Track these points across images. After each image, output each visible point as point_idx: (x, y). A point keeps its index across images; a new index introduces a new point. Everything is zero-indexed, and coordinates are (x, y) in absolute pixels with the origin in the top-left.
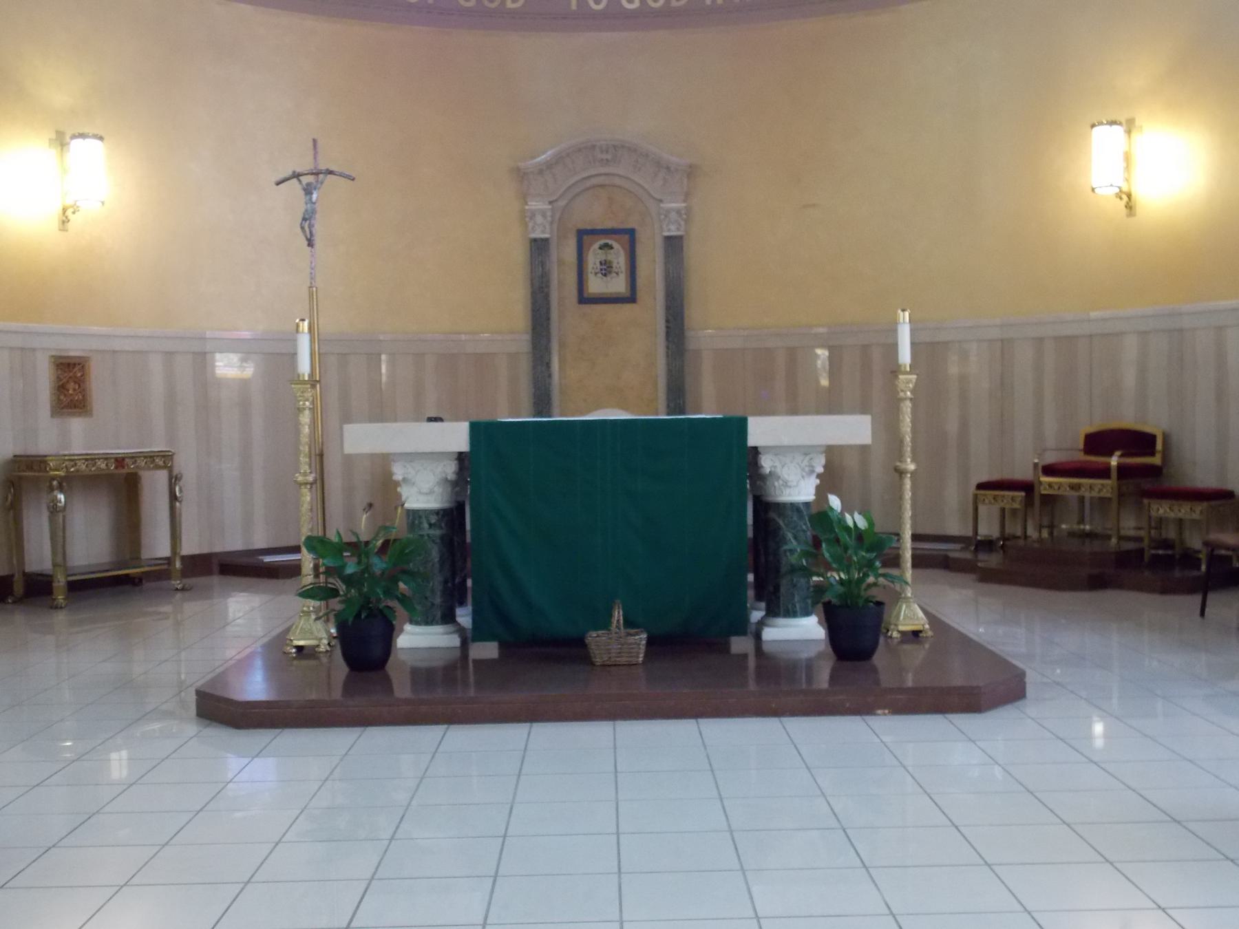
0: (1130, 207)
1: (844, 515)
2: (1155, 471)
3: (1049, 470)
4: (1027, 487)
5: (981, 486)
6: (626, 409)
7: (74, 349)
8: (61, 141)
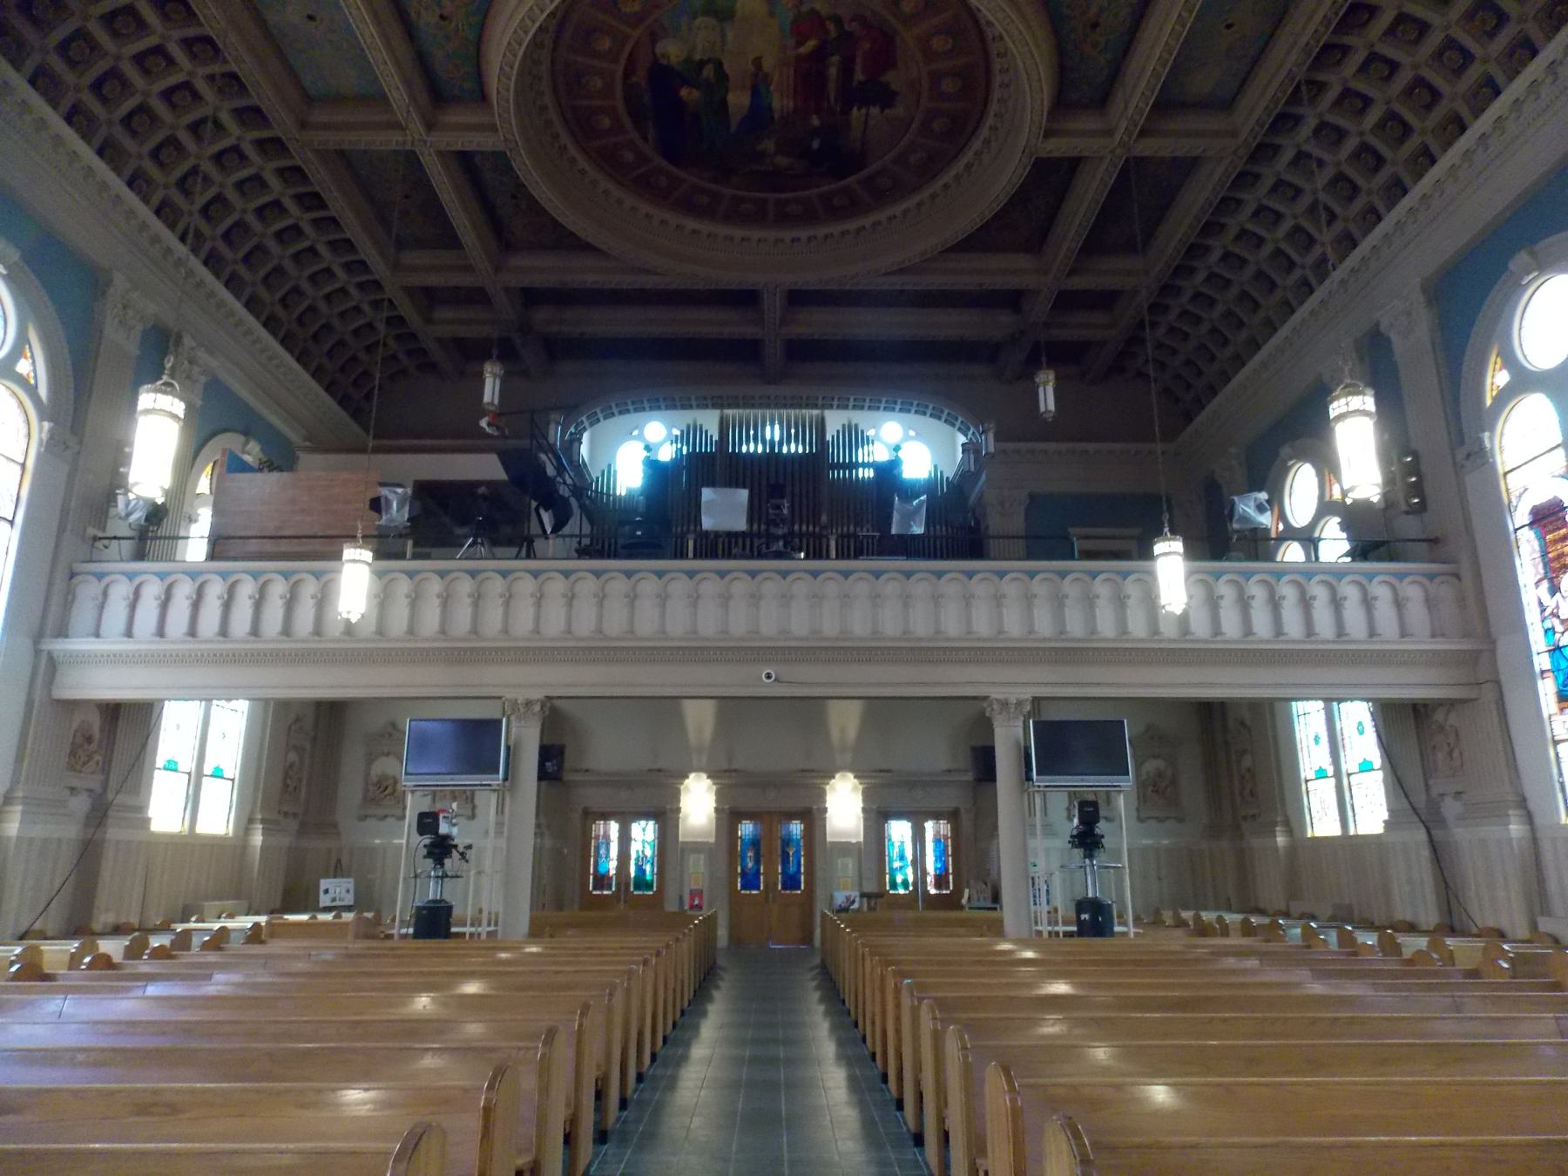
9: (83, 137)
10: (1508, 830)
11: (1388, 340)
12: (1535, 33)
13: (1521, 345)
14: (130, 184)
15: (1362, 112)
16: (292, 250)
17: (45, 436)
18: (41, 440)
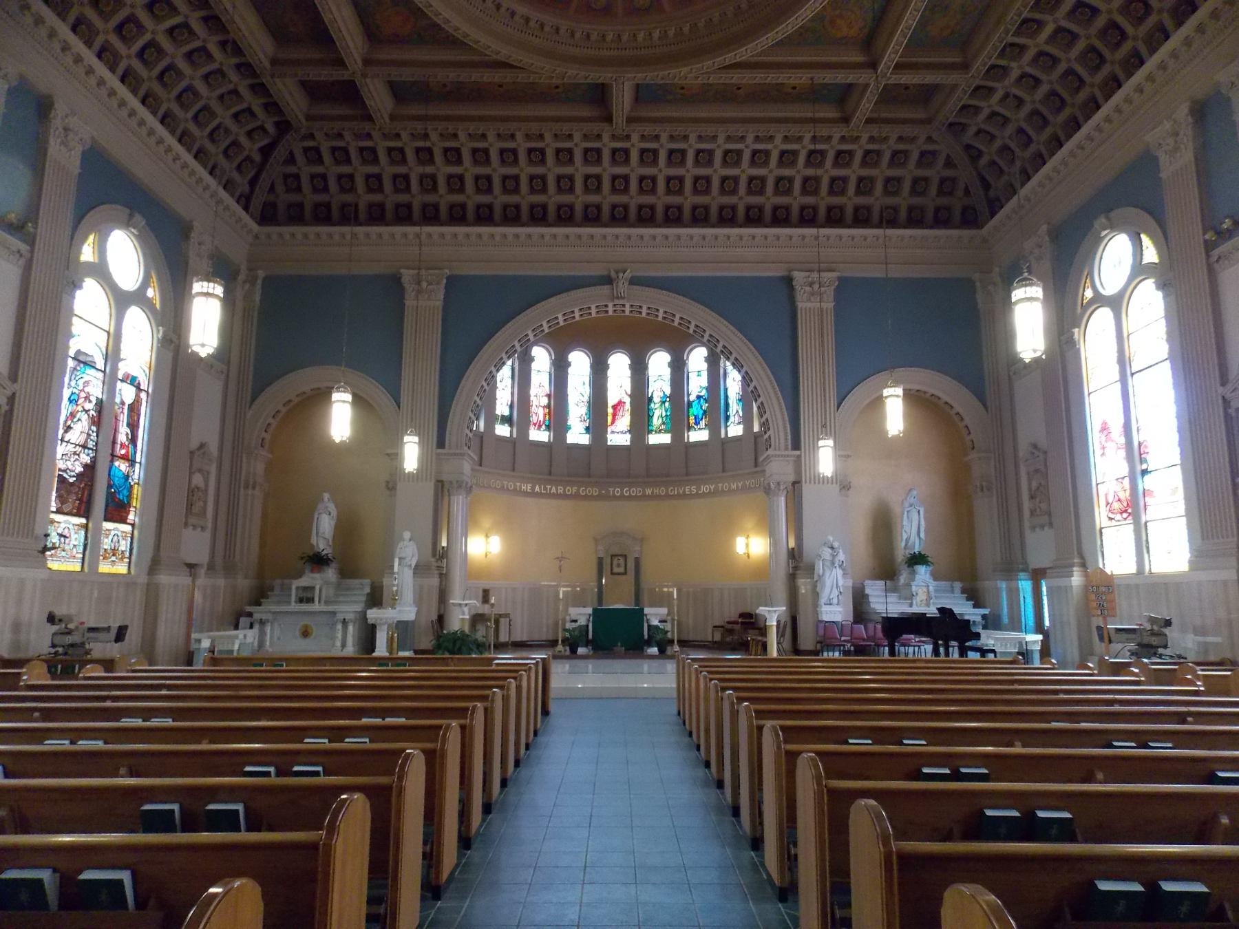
0: (748, 556)
1: (1208, 888)
2: (753, 623)
3: (729, 623)
4: (722, 627)
5: (714, 627)
6: (624, 604)
7: (487, 587)
8: (487, 536)
9: (59, 15)
10: (1071, 581)
11: (1156, 159)
12: (1168, 23)
13: (1101, 284)
14: (143, 102)
15: (1090, 21)
16: (219, 92)
17: (160, 335)
18: (158, 339)
